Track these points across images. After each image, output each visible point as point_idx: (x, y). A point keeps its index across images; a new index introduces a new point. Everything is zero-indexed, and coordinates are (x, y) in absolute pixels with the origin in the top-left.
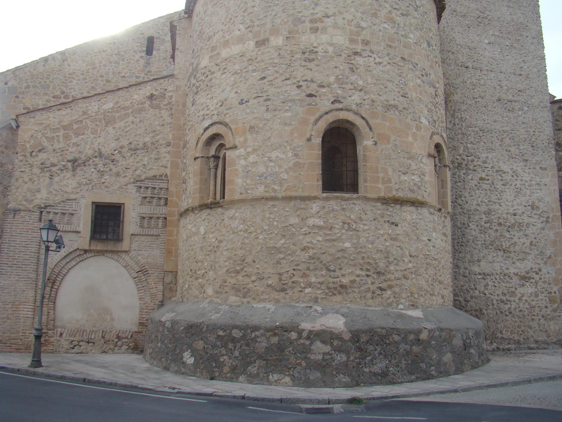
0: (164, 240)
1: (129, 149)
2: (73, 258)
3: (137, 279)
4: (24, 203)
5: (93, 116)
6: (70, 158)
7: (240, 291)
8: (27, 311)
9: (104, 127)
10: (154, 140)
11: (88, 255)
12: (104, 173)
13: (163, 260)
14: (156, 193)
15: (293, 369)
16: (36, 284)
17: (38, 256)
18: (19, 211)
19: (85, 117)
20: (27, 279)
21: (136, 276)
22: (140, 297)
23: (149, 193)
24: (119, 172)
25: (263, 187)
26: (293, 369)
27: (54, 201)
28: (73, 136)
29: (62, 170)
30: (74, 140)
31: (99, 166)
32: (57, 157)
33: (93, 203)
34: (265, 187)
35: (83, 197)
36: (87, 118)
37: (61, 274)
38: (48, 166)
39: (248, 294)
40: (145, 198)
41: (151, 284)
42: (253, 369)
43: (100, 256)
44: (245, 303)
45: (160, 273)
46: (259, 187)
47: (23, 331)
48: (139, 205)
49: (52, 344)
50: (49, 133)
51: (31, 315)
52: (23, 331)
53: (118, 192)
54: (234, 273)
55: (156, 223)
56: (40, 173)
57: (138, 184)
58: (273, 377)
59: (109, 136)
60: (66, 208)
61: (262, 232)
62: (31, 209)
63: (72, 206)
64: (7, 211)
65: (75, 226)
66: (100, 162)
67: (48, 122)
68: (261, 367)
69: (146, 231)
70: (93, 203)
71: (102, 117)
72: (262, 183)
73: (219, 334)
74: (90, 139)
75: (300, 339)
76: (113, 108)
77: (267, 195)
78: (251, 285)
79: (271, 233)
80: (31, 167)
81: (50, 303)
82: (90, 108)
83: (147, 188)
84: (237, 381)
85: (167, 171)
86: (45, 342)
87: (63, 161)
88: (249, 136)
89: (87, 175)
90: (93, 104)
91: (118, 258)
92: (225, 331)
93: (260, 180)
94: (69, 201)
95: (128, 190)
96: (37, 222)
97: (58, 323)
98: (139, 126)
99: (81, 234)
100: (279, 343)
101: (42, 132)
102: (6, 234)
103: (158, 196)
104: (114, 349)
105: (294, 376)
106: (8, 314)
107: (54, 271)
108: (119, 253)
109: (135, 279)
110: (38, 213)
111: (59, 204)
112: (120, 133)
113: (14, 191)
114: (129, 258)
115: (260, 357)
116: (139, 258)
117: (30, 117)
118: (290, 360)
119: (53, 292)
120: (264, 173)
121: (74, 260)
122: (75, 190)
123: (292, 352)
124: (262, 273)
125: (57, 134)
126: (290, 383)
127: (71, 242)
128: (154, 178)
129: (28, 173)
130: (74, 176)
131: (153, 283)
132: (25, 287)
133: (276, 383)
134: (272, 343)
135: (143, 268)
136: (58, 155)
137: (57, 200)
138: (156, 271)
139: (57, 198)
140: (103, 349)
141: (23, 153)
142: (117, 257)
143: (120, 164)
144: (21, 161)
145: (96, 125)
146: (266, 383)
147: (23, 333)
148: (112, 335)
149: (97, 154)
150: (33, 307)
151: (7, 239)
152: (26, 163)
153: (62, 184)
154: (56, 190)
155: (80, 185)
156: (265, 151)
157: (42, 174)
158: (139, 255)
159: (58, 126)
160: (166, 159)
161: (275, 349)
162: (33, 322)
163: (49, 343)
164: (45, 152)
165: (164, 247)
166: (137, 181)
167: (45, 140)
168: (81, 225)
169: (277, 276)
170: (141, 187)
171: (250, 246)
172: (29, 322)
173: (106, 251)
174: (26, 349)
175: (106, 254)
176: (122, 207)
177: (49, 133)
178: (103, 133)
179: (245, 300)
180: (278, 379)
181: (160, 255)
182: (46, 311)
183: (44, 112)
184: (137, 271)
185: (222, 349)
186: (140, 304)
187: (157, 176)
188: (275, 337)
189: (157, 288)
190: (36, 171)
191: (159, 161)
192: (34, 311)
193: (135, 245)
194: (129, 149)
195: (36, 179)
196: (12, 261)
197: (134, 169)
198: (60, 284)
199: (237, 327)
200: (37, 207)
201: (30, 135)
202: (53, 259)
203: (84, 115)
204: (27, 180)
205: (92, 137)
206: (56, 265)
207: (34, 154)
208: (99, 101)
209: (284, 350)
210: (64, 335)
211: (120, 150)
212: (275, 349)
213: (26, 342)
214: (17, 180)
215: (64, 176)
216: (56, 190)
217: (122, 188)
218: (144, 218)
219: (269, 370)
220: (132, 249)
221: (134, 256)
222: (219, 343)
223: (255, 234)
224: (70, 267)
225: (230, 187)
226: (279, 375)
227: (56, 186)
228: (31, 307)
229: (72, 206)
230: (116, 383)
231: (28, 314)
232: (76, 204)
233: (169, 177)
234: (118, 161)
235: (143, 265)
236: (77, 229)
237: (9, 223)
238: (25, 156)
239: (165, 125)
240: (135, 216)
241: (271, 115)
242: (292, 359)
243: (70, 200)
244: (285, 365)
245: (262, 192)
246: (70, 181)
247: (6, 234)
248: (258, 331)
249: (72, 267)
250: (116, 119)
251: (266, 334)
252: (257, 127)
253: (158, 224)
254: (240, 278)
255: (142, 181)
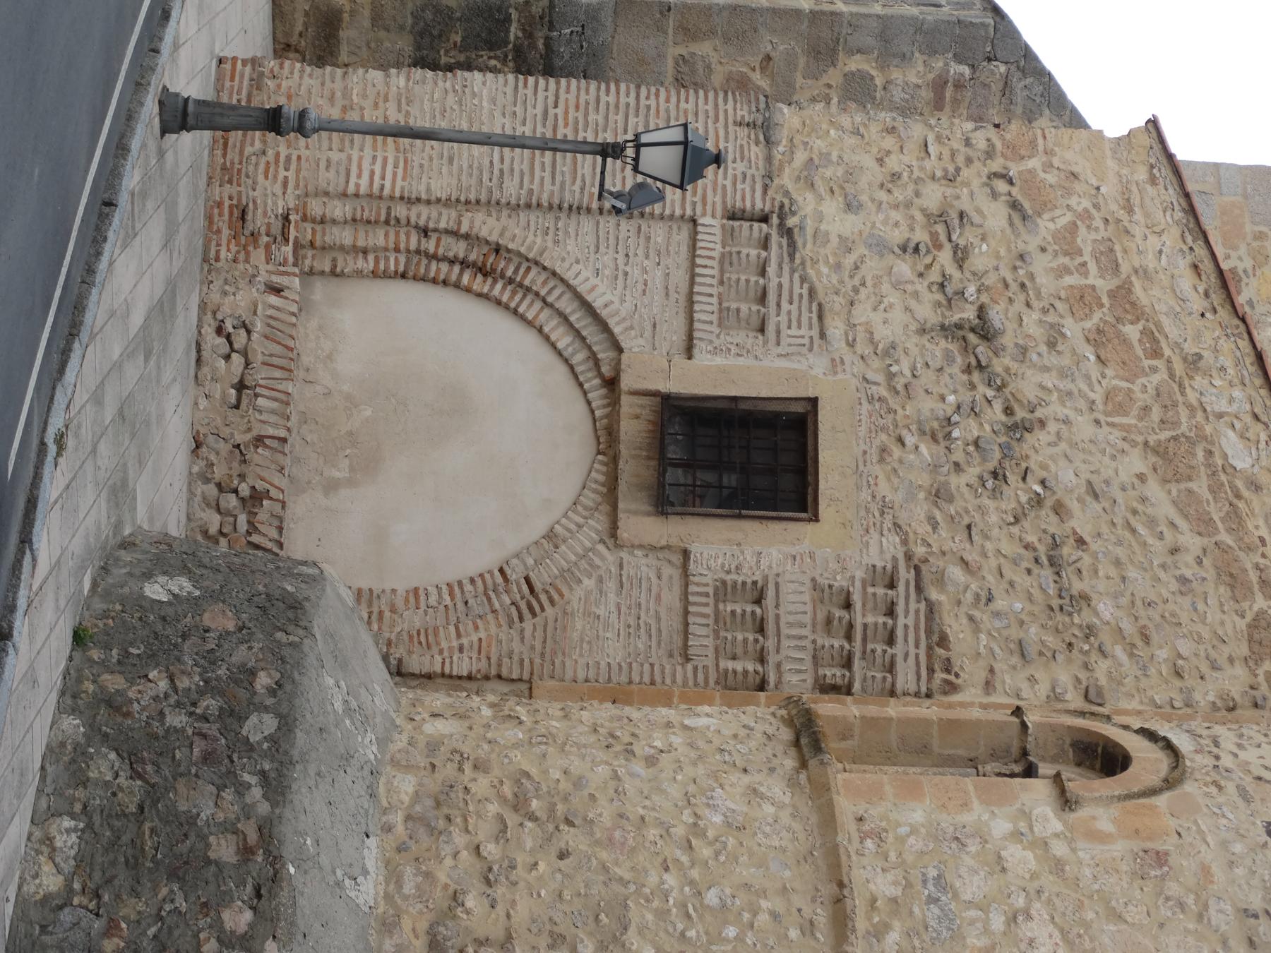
0: (668, 681)
1: (1053, 537)
2: (583, 339)
3: (499, 579)
4: (800, 157)
5: (1183, 394)
6: (996, 315)
7: (438, 804)
8: (372, 173)
9: (1140, 439)
10: (1105, 637)
11: (597, 397)
12: (943, 444)
13: (581, 675)
14: (870, 646)
15: (92, 906)
16: (478, 202)
17: (589, 210)
18: (767, 140)
19: (1179, 368)
20: (496, 172)
21: (513, 577)
22: (421, 593)
23: (870, 619)
24: (951, 500)
25: (897, 892)
26: (92, 906)
27: (815, 262)
28: (1088, 324)
29: (942, 286)
30: (1072, 328)
31: (972, 423)
32: (997, 269)
33: (814, 402)
34: (894, 900)
35: (836, 365)
36: (1172, 376)
37: (517, 298)
38: (954, 237)
39: (422, 830)
40: (848, 606)
41: (476, 628)
42: (105, 765)
43: (592, 441)
44: (384, 819)
45: (522, 661)
46: (890, 877)
47: (294, 158)
48: (813, 580)
49: (242, 256)
50: (1093, 236)
51: (358, 185)
52: (294, 158)
53: (865, 495)
54: (516, 795)
55: (739, 651)
56: (923, 210)
57: (905, 575)
58: (68, 831)
59: (1107, 460)
60: (785, 306)
61: (692, 883)
62: (776, 181)
63: (794, 323)
64: (762, 99)
65: (713, 337)
66: (987, 428)
67: (1137, 231)
68: (114, 794)
69: (703, 609)
70: (814, 402)
71: (1184, 428)
72: (909, 885)
73: (262, 674)
74: (1084, 387)
75: (219, 940)
76: (1229, 468)
77: (858, 903)
78: (459, 839)
79: (689, 916)
80: (945, 177)
81: (402, 259)
82: (1217, 382)
83: (891, 612)
84: (60, 710)
85: (973, 691)
86: (247, 232)
87: (979, 291)
88: (1119, 848)
89: (927, 378)
90: (1237, 393)
91: (586, 508)
92: (272, 692)
93: (925, 882)
94: (814, 316)
95: (875, 535)
96: (724, 202)
97: (320, 290)
98: (1162, 574)
99: (679, 360)
100: (208, 862)
101: (1093, 211)
102: (674, 99)
103: (858, 655)
104: (207, 481)
105: (61, 908)
106: (362, 109)
107: (529, 269)
108: (605, 508)
109: (497, 573)
110: (759, 205)
111: (803, 280)
112: (1120, 501)
113: (845, 121)
114: (588, 544)
115: (154, 794)
116: (586, 581)
117: (1152, 167)
118: (133, 900)
119: (444, 267)
120: (956, 896)
121: (577, 344)
122: (861, 336)
123: (168, 907)
124: (513, 878)
125: (1092, 267)
126: (33, 889)
127: (649, 328)
128: (935, 638)
129: (922, 168)
130: (922, 331)
131: (482, 635)
132: (465, 166)
133: (41, 842)
134: (212, 839)
135: (543, 597)
136: (1006, 273)
137: (819, 273)
138: (533, 648)
139: (825, 270)
140: (211, 439)
141: (999, 145)
142: (591, 504)
143: (986, 501)
144: (968, 142)
145: (1146, 409)
146: (43, 803)
147: (288, 158)
148: (265, 474)
149: (1020, 414)
150: (386, 192)
151: (652, 102)
152: (960, 160)
153: (886, 288)
154: (857, 268)
155: (887, 353)
156: (1057, 901)
157: (919, 216)
158: (600, 580)
159: (1125, 268)
160: (1025, 686)
161: (183, 848)
162: (327, 194)
163: (245, 247)
164: (1011, 224)
165: (636, 678)
166: (917, 568)
167: (1062, 222)
168: (719, 360)
169: (497, 933)
170: (892, 585)
171: (631, 842)
172: (328, 179)
173: (615, 459)
174: (224, 168)
175: (602, 463)
176: (803, 515)
177: (1093, 236)
178: (1115, 436)
179: (398, 819)
180: (54, 849)
181: (603, 664)
182: (371, 243)
183: (1179, 215)
184: (532, 575)
185: (197, 678)
186: (394, 591)
187: (948, 649)
188: (237, 853)
189: (461, 649)
190: (933, 196)
191: (1015, 660)
192: (370, 196)
193: (640, 565)
194: (1053, 537)
195: (898, 195)
196: (566, 118)
197: (968, 557)
198: (480, 295)
199: (287, 724)
200: (786, 202)
201: (1075, 169)
202: (577, 262)
203: (1185, 359)
204: (893, 163)
205: (1092, 395)
206: (554, 274)
207: (1002, 186)
208: (1256, 417)
209: (181, 880)
210: (273, 299)
211: (1049, 503)
212: (183, 848)
213: (251, 168)
214: (891, 130)
215: (916, 295)
216: (857, 268)
217: (882, 513)
218: (758, 601)
219: (97, 819)
220: (624, 555)
221: (597, 561)
222: (222, 672)
223: (685, 859)
224: (546, 329)
225: (887, 788)
226: (73, 853)
227: (872, 266)
228: (388, 184)
229: (794, 323)
230: (91, 284)
231: (359, 176)
232: (806, 341)
233: (946, 699)
234: (996, 494)
235: (556, 597)
236: (700, 347)
237: (716, 105)
238: (990, 154)
239: (1177, 683)
240: (764, 563)
241: (1223, 927)
242: (132, 908)
243: (820, 317)
244: (115, 877)
245: (872, 886)
246: (898, 316)
247: (674, 99)
248: (264, 796)
249: (547, 338)
250: (1183, 486)
251: (253, 820)
252: (1163, 878)
253: (734, 658)
254: (493, 808)
255: (919, 589)
